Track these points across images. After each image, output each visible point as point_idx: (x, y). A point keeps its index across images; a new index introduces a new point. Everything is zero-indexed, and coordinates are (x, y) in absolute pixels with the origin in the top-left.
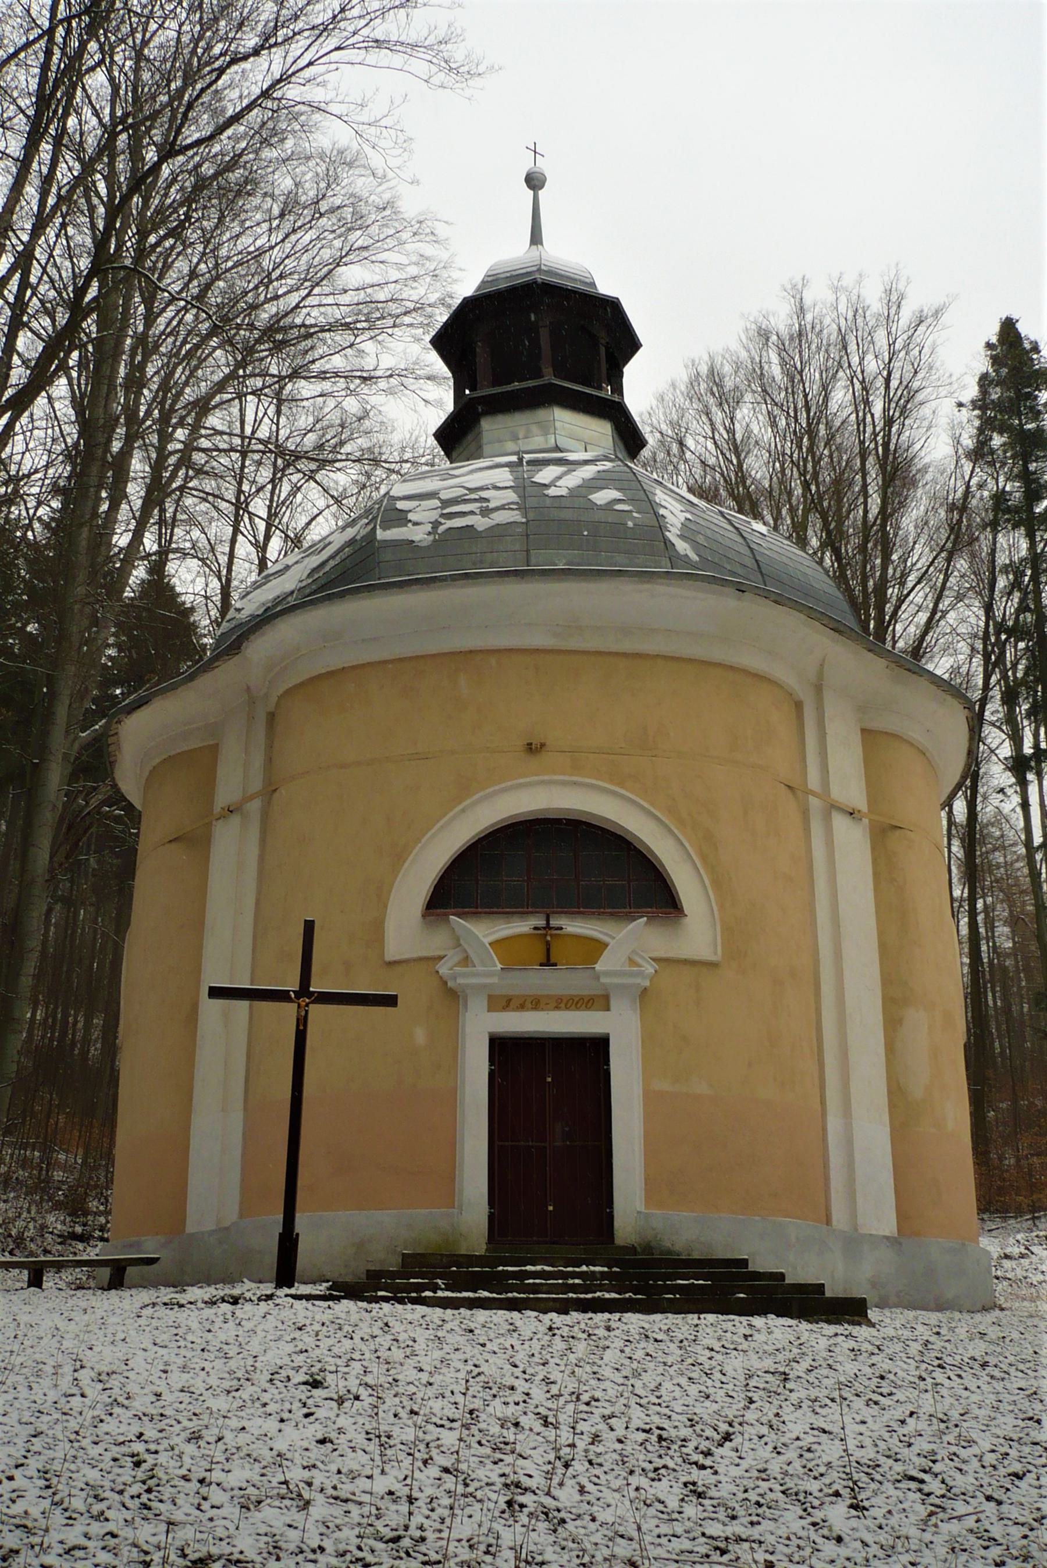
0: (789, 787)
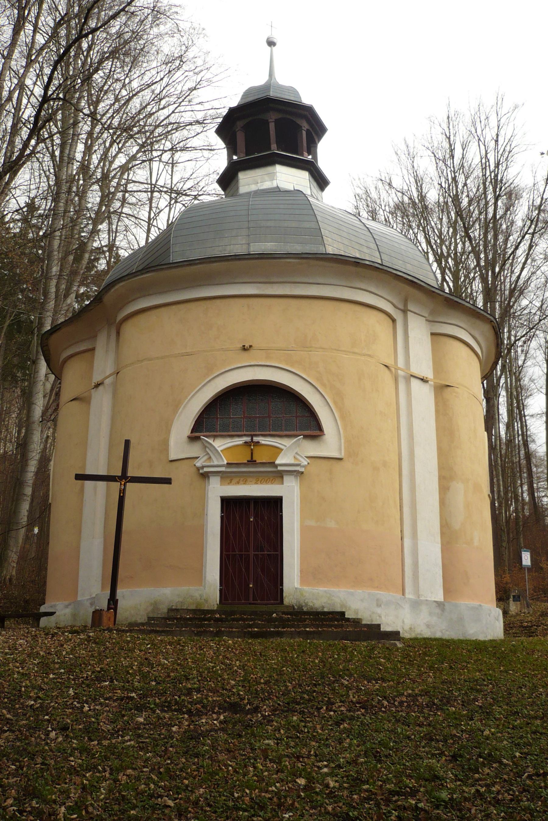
0: (386, 366)
